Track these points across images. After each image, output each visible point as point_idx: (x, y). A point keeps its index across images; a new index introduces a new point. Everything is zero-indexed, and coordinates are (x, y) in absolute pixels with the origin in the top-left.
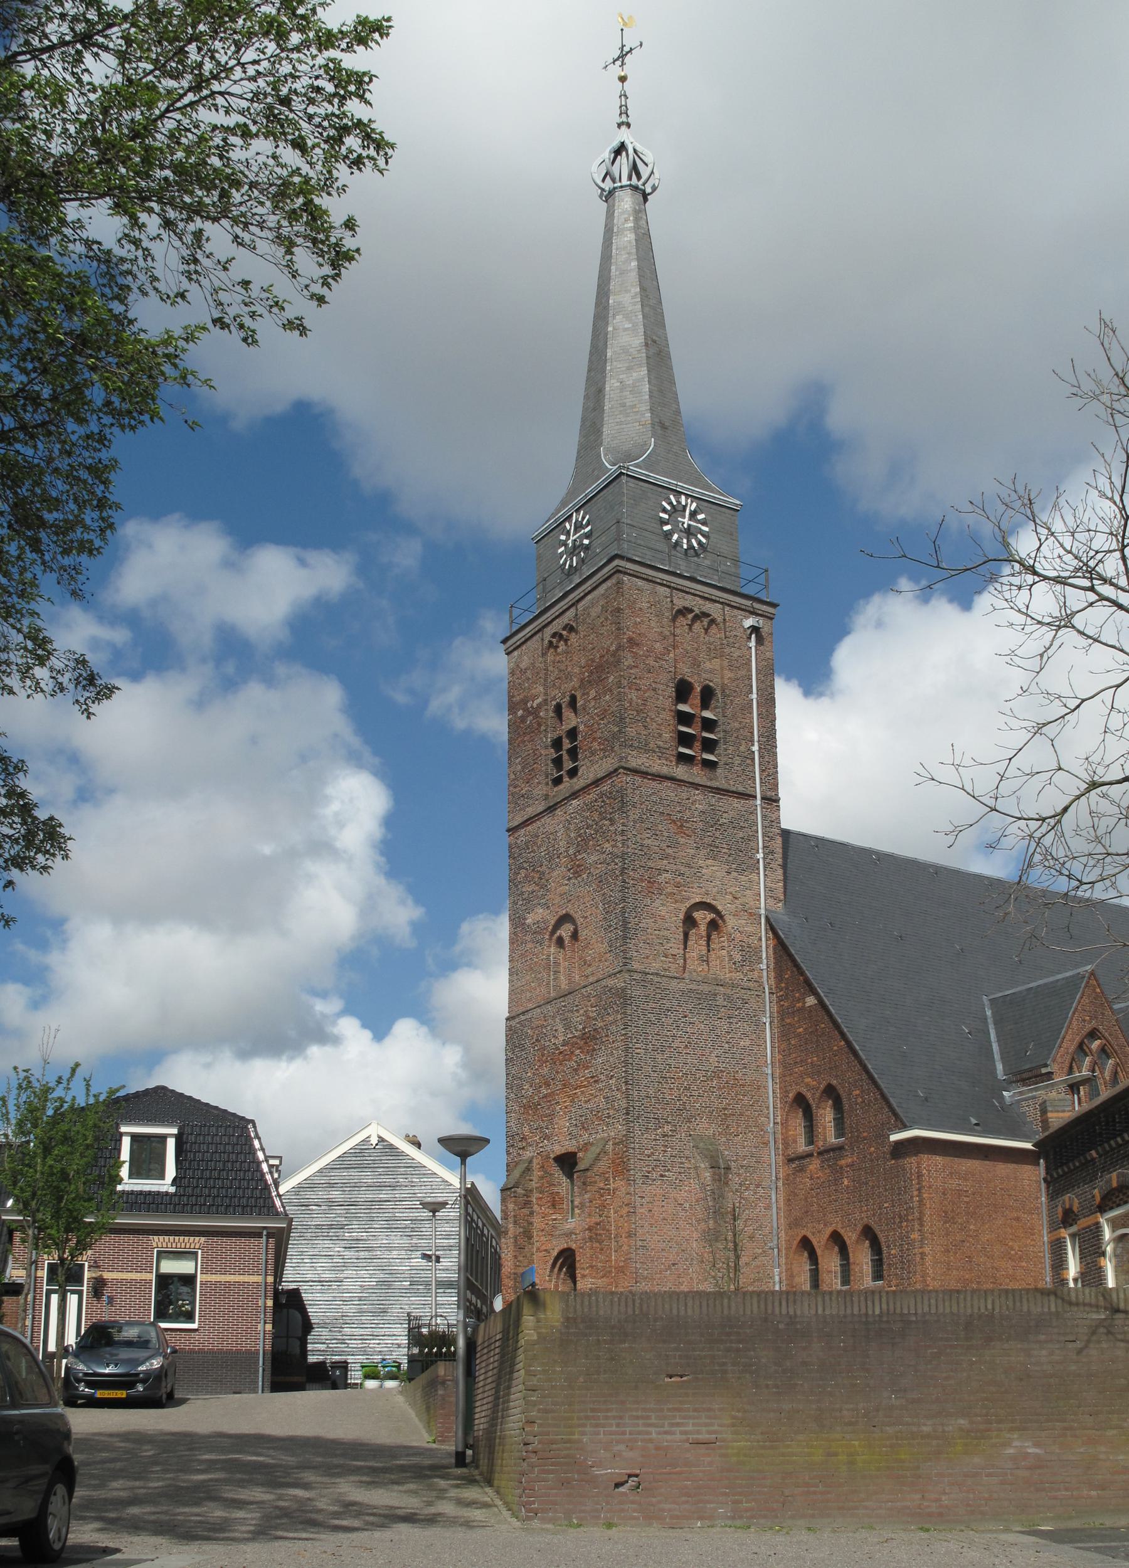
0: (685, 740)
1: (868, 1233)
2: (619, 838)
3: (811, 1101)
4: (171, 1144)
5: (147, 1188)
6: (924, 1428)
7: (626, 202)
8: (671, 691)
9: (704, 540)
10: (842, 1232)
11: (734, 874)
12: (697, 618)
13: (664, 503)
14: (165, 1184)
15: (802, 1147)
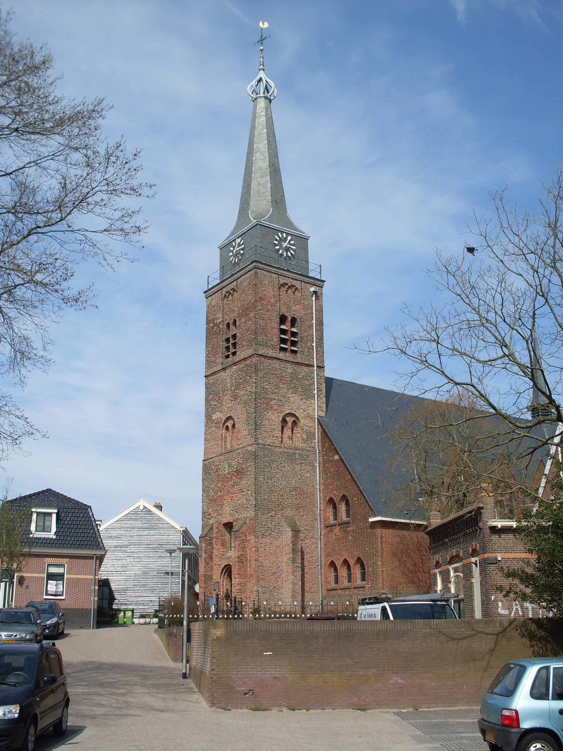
0: (283, 341)
1: (359, 561)
2: (254, 385)
3: (336, 501)
4: (54, 517)
5: (43, 536)
6: (360, 673)
7: (262, 103)
8: (278, 320)
9: (293, 253)
10: (348, 559)
11: (304, 400)
12: (290, 287)
13: (276, 237)
14: (51, 535)
15: (332, 521)
